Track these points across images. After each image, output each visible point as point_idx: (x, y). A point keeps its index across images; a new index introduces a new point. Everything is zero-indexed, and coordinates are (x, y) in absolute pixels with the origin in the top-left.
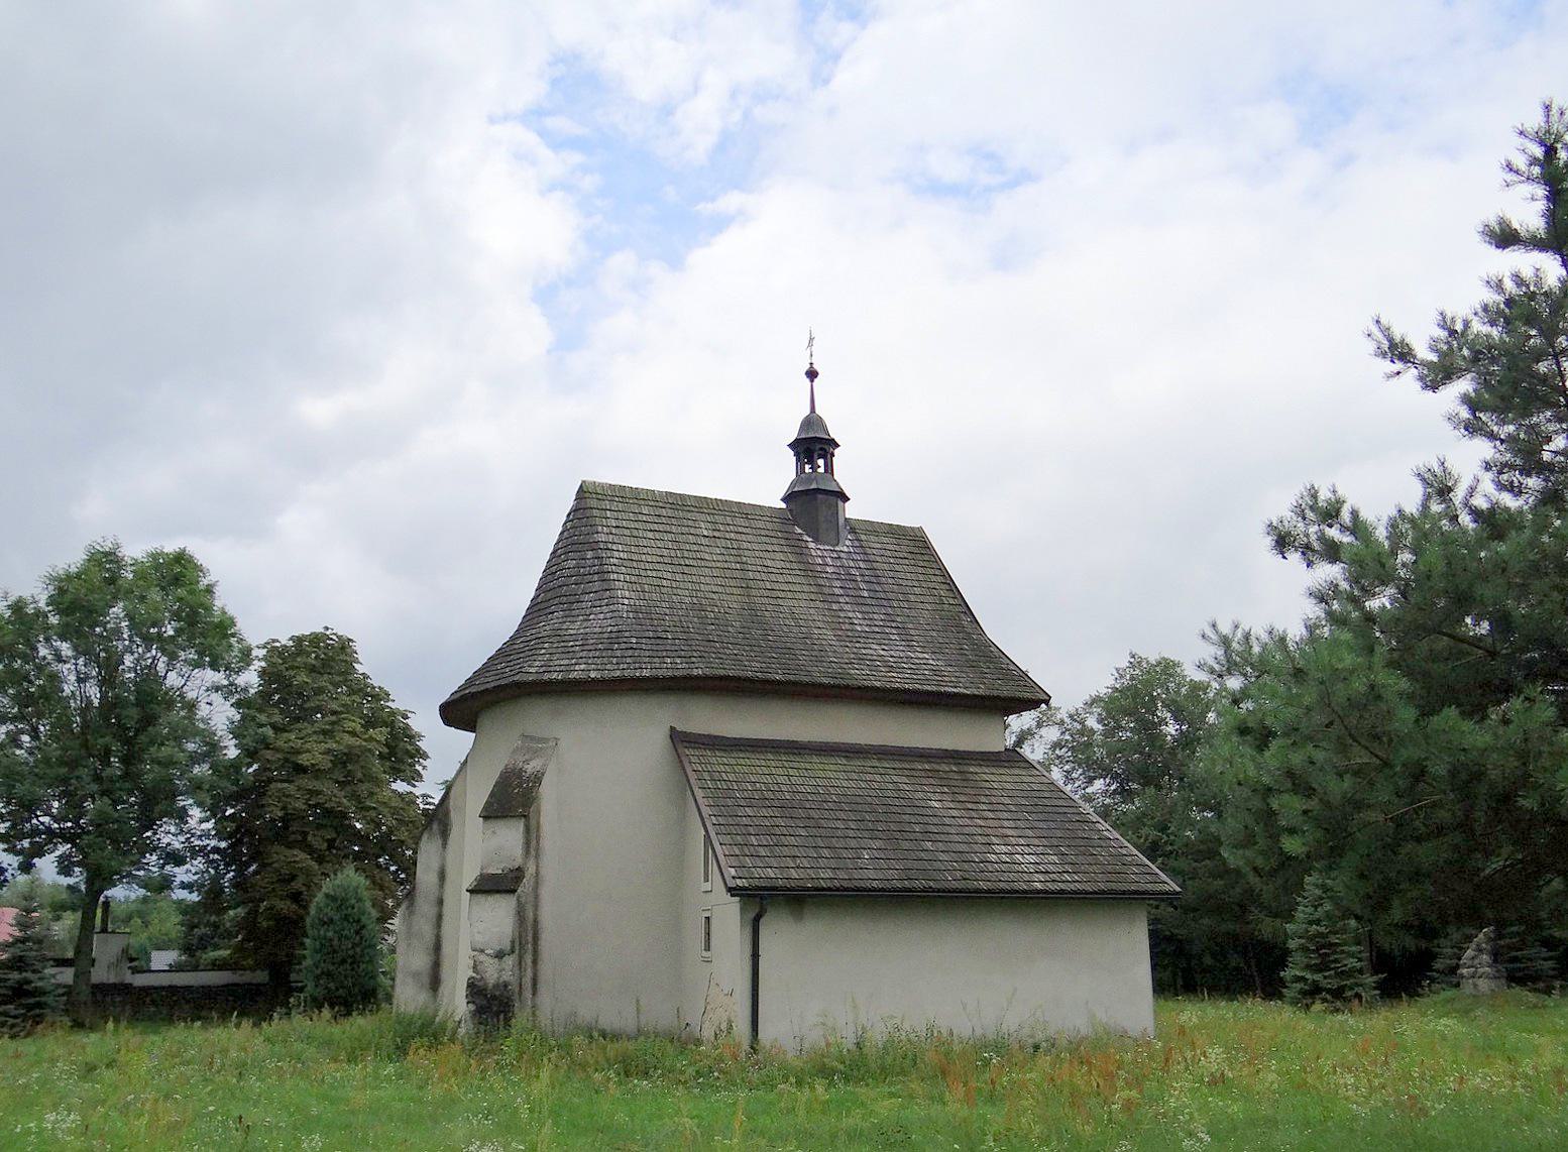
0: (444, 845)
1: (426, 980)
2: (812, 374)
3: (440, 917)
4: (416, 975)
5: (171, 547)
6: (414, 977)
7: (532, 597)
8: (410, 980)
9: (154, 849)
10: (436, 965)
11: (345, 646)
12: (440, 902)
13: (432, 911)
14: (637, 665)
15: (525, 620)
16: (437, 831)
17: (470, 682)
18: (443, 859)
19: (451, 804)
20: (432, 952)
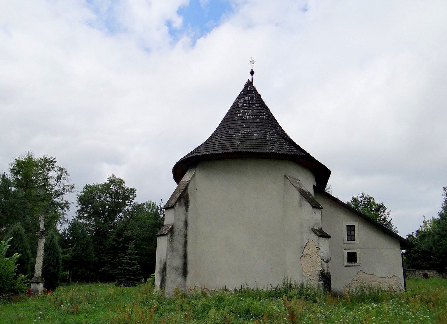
0: (187, 210)
1: (181, 271)
2: (252, 73)
3: (186, 243)
4: (176, 269)
5: (250, 74)
6: (175, 269)
7: (212, 134)
8: (173, 271)
9: (28, 249)
10: (185, 265)
11: (254, 73)
12: (186, 236)
13: (182, 240)
14: (290, 148)
15: (221, 125)
16: (184, 203)
17: (192, 153)
18: (187, 216)
19: (189, 192)
20: (182, 258)
